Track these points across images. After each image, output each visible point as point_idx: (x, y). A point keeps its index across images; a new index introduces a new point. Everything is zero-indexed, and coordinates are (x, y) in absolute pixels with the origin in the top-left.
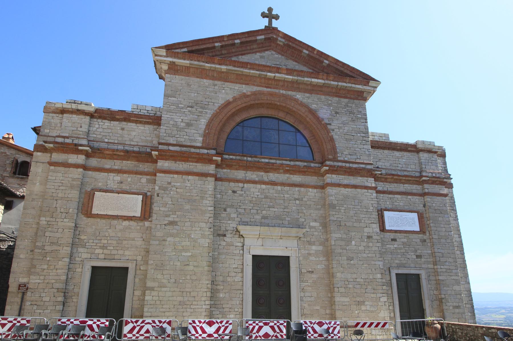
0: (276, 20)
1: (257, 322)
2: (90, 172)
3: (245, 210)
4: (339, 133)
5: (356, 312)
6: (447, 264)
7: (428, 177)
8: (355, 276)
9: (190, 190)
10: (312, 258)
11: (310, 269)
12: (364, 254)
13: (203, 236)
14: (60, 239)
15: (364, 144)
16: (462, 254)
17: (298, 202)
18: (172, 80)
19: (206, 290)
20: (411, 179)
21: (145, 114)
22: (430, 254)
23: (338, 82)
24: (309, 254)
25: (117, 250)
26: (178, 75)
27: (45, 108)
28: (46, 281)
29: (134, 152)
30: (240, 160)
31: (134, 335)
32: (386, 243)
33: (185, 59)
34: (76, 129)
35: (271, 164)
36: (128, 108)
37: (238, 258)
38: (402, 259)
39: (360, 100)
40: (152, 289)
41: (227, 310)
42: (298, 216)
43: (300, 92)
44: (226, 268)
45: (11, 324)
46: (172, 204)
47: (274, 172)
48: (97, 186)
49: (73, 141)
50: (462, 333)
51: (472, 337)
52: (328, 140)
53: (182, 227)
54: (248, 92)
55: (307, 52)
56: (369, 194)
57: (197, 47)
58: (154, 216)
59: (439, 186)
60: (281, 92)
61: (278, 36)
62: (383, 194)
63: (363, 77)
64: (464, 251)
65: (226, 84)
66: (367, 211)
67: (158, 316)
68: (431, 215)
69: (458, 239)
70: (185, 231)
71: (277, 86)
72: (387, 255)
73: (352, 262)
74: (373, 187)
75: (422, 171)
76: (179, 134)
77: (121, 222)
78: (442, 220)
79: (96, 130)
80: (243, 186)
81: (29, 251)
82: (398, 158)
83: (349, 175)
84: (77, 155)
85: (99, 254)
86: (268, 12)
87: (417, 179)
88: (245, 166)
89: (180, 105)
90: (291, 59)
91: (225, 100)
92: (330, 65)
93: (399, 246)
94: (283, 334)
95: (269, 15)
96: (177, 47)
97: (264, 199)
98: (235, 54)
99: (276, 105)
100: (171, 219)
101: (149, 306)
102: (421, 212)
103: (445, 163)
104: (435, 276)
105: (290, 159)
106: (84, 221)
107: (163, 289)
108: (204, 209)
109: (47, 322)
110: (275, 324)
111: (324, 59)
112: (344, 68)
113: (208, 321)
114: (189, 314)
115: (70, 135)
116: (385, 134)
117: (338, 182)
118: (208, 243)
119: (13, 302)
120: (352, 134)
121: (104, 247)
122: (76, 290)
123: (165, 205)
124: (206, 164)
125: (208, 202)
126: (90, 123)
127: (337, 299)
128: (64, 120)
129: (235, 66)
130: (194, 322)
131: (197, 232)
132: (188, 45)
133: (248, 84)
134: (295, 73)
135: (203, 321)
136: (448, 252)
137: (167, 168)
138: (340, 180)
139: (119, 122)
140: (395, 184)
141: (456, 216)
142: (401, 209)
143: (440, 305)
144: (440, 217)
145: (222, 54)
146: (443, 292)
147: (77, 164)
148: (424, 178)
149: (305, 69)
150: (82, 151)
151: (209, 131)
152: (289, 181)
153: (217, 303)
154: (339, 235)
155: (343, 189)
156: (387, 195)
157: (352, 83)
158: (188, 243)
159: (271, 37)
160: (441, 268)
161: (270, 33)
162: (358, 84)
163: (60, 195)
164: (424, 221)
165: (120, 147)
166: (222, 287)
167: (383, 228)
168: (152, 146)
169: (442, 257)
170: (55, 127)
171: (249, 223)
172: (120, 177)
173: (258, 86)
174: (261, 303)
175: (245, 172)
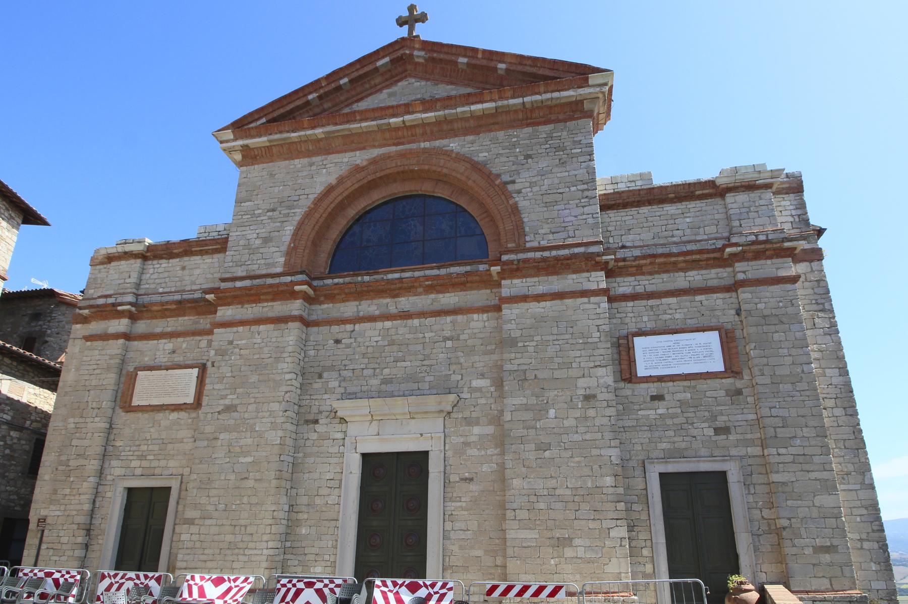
0: (423, 22)
1: (295, 581)
2: (136, 343)
4: (530, 194)
5: (552, 562)
6: (798, 442)
7: (740, 246)
8: (552, 483)
9: (260, 348)
10: (473, 452)
11: (467, 474)
12: (576, 436)
13: (274, 426)
14: (87, 449)
15: (583, 204)
16: (851, 415)
17: (449, 344)
18: (249, 174)
19: (270, 522)
20: (698, 257)
22: (752, 422)
23: (523, 97)
25: (159, 460)
26: (258, 164)
28: (66, 513)
32: (637, 407)
33: (260, 136)
34: (122, 281)
38: (676, 439)
39: (580, 118)
40: (191, 522)
41: (312, 557)
42: (449, 370)
43: (456, 136)
44: (315, 480)
46: (232, 377)
47: (407, 294)
52: (508, 213)
56: (592, 306)
57: (282, 111)
59: (774, 261)
60: (422, 145)
62: (633, 301)
63: (578, 71)
64: (858, 407)
66: (586, 343)
67: (196, 568)
70: (248, 419)
71: (414, 138)
73: (547, 454)
77: (168, 414)
78: (783, 339)
80: (352, 329)
82: (673, 217)
83: (547, 275)
89: (256, 212)
91: (327, 185)
92: (510, 70)
93: (670, 411)
95: (412, 19)
96: (250, 119)
97: (386, 348)
98: (345, 103)
99: (412, 171)
100: (227, 402)
101: (184, 551)
102: (729, 327)
103: (802, 206)
106: (122, 417)
107: (208, 522)
108: (278, 378)
111: (495, 62)
112: (537, 67)
113: (409, 581)
116: (641, 175)
117: (524, 291)
118: (281, 437)
120: (559, 191)
121: (142, 457)
123: (221, 379)
124: (288, 300)
125: (286, 365)
126: (143, 269)
127: (511, 534)
128: (111, 271)
129: (336, 124)
131: (264, 420)
132: (266, 112)
133: (364, 148)
134: (439, 105)
135: (207, 577)
142: (677, 327)
149: (469, 90)
150: (123, 312)
152: (437, 307)
154: (522, 400)
156: (644, 302)
157: (552, 91)
158: (249, 441)
159: (402, 55)
160: (779, 454)
161: (399, 49)
163: (94, 383)
164: (736, 347)
165: (177, 297)
166: (305, 516)
169: (783, 427)
170: (101, 284)
172: (172, 344)
174: (373, 544)
175: (357, 303)
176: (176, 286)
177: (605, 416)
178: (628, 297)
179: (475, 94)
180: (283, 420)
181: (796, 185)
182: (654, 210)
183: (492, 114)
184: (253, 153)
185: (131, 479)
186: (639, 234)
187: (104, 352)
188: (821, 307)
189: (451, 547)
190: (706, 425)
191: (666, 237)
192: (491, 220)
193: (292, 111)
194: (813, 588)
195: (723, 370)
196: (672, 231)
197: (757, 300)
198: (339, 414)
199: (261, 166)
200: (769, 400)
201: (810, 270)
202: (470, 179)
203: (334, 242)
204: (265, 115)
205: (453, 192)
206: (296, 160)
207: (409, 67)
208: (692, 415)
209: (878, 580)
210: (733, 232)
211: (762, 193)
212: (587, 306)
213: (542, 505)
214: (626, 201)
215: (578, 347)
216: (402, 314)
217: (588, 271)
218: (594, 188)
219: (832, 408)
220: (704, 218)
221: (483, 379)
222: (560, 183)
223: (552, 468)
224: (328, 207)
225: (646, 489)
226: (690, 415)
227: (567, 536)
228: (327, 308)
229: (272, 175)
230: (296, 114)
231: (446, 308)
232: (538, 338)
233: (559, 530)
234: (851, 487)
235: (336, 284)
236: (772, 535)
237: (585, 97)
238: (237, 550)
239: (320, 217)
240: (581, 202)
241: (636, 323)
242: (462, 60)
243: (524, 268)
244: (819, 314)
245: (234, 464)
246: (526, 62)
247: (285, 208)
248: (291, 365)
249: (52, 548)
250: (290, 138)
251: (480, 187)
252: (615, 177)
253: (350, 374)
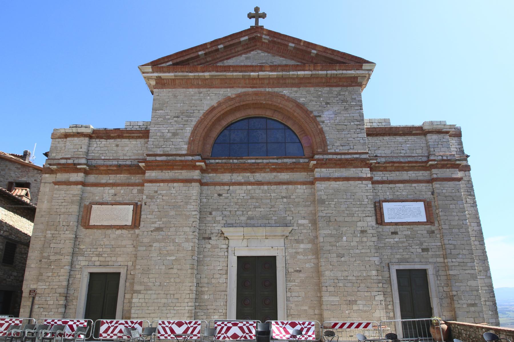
0: (264, 18)
1: (226, 323)
2: (89, 188)
3: (230, 213)
4: (329, 124)
5: (347, 312)
6: (461, 256)
7: (436, 161)
8: (346, 274)
10: (300, 257)
12: (357, 250)
13: (187, 240)
14: (62, 249)
17: (285, 200)
18: (160, 94)
19: (189, 292)
20: (415, 164)
21: (137, 129)
23: (327, 71)
24: (297, 253)
26: (166, 88)
27: (53, 134)
28: (51, 287)
29: (125, 166)
30: (226, 163)
31: (109, 335)
32: (384, 237)
33: (169, 72)
34: (77, 150)
35: (256, 164)
36: (122, 126)
37: (223, 259)
38: (404, 253)
39: (355, 86)
41: (212, 311)
42: (286, 214)
43: (287, 87)
45: (7, 324)
46: (158, 211)
48: (94, 200)
49: (74, 161)
50: (466, 334)
51: (474, 339)
52: (317, 133)
53: (167, 233)
54: (233, 95)
55: (293, 45)
57: (182, 59)
58: (142, 224)
59: (450, 169)
60: (267, 90)
61: (263, 34)
62: (382, 184)
63: (356, 61)
65: (212, 90)
66: (360, 204)
67: (144, 318)
68: (440, 202)
69: (476, 228)
71: (262, 85)
72: (387, 250)
73: (343, 259)
74: (369, 177)
75: (430, 155)
76: (166, 144)
77: (114, 231)
78: (454, 207)
79: (95, 149)
80: (228, 189)
81: (38, 261)
82: (401, 143)
83: (340, 168)
84: (77, 174)
85: (95, 261)
86: (255, 12)
87: (423, 164)
88: (230, 169)
89: (166, 117)
90: (278, 55)
92: (319, 54)
93: (401, 240)
94: (252, 335)
95: (257, 15)
97: (249, 200)
98: (220, 59)
99: (261, 104)
100: (156, 225)
102: (428, 200)
103: (461, 143)
104: (446, 270)
105: (277, 157)
106: (83, 232)
108: (188, 213)
109: (35, 322)
110: (244, 325)
111: (311, 49)
112: (334, 55)
114: (173, 315)
115: (72, 157)
116: (384, 119)
117: (328, 175)
118: (192, 246)
119: (25, 305)
120: (344, 124)
121: (99, 255)
122: (75, 294)
125: (192, 207)
126: (89, 144)
127: (325, 299)
128: (68, 143)
129: (217, 71)
130: (163, 323)
131: (181, 237)
132: (172, 58)
133: (233, 87)
134: (279, 68)
136: (461, 243)
137: (154, 178)
138: (330, 173)
139: (114, 139)
140: (397, 173)
141: (475, 202)
142: (404, 199)
143: (451, 303)
144: (451, 204)
145: (207, 62)
146: (454, 289)
147: (77, 181)
148: (430, 163)
150: (80, 169)
151: (194, 138)
153: (202, 305)
154: (329, 232)
155: (333, 183)
156: (387, 185)
157: (343, 70)
158: (172, 248)
159: (255, 36)
160: (452, 262)
162: (350, 70)
163: (63, 210)
164: (432, 210)
165: (115, 163)
166: (207, 289)
167: (382, 221)
168: (143, 158)
169: (454, 249)
170: (60, 151)
171: (235, 225)
172: (114, 190)
173: (243, 87)
175: (231, 174)
176: (113, 156)
178: (380, 182)
179: (301, 66)
180: (192, 237)
181: (458, 133)
182: (392, 139)
183: (308, 77)
185: (93, 267)
186: (384, 150)
187: (68, 192)
188: (469, 193)
189: (292, 305)
191: (397, 153)
192: (306, 136)
193: (188, 60)
195: (426, 221)
197: (442, 188)
198: (225, 235)
200: (448, 236)
201: (464, 175)
202: (295, 112)
204: (171, 60)
206: (190, 89)
208: (411, 242)
209: (492, 318)
210: (431, 154)
211: (444, 135)
213: (341, 284)
214: (378, 133)
215: (357, 206)
216: (256, 182)
217: (361, 167)
218: (363, 124)
219: (474, 241)
220: (416, 145)
221: (305, 219)
222: (345, 120)
223: (345, 266)
224: (212, 118)
225: (390, 277)
226: (410, 242)
227: (354, 300)
228: (212, 176)
230: (190, 62)
232: (336, 200)
233: (350, 297)
234: (482, 277)
235: (217, 163)
236: (448, 299)
238: (169, 307)
239: (208, 124)
240: (356, 131)
241: (383, 195)
242: (291, 45)
244: (469, 197)
245: (164, 260)
246: (327, 51)
247: (185, 117)
248: (195, 207)
249: (42, 308)
250: (189, 76)
251: (302, 117)
252: (371, 119)
253: (228, 213)
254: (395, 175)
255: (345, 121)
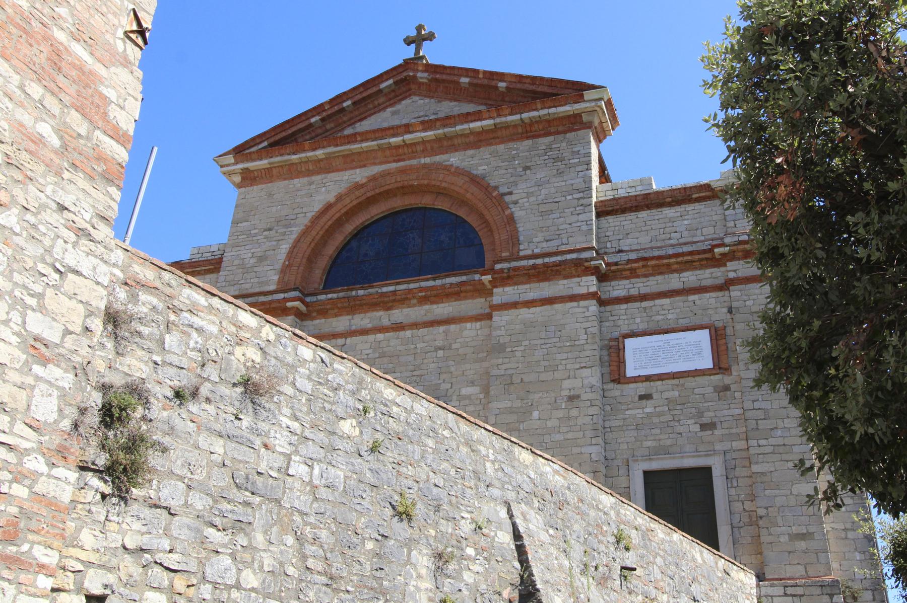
0: (431, 40)
6: (779, 433)
7: (727, 246)
15: (578, 212)
17: (440, 353)
20: (689, 258)
23: (521, 113)
33: (261, 159)
38: (662, 437)
39: (580, 129)
42: (439, 379)
43: (456, 151)
57: (284, 134)
60: (423, 161)
80: (343, 343)
82: (672, 220)
83: (540, 281)
87: (707, 255)
90: (446, 99)
91: (325, 203)
93: (657, 409)
95: (419, 39)
96: (252, 144)
97: (377, 360)
98: (348, 123)
99: (412, 186)
102: (720, 324)
112: (535, 84)
116: (641, 180)
117: (515, 298)
120: (555, 200)
129: (337, 145)
132: (268, 136)
133: (365, 166)
134: (438, 124)
140: (659, 278)
145: (327, 131)
149: (470, 108)
152: (430, 317)
154: (507, 404)
156: (637, 304)
159: (406, 77)
169: (765, 419)
173: (381, 163)
175: (350, 317)
177: (587, 415)
184: (252, 175)
190: (693, 421)
191: (663, 240)
193: (294, 134)
194: (788, 575)
195: (711, 366)
196: (670, 233)
197: (746, 298)
199: (260, 187)
202: (468, 192)
203: (330, 257)
205: (452, 205)
206: (296, 180)
207: (413, 86)
208: (679, 412)
212: (577, 310)
216: (394, 326)
217: (578, 276)
226: (676, 412)
229: (270, 195)
231: (439, 318)
232: (526, 343)
235: (331, 299)
236: (752, 527)
237: (583, 111)
242: (464, 80)
243: (514, 275)
254: (655, 282)
255: (557, 195)
